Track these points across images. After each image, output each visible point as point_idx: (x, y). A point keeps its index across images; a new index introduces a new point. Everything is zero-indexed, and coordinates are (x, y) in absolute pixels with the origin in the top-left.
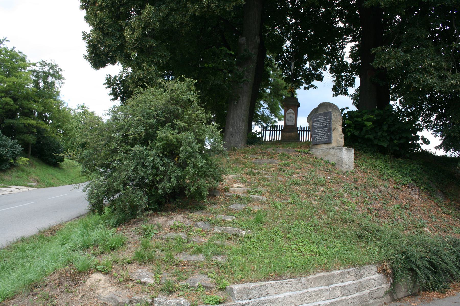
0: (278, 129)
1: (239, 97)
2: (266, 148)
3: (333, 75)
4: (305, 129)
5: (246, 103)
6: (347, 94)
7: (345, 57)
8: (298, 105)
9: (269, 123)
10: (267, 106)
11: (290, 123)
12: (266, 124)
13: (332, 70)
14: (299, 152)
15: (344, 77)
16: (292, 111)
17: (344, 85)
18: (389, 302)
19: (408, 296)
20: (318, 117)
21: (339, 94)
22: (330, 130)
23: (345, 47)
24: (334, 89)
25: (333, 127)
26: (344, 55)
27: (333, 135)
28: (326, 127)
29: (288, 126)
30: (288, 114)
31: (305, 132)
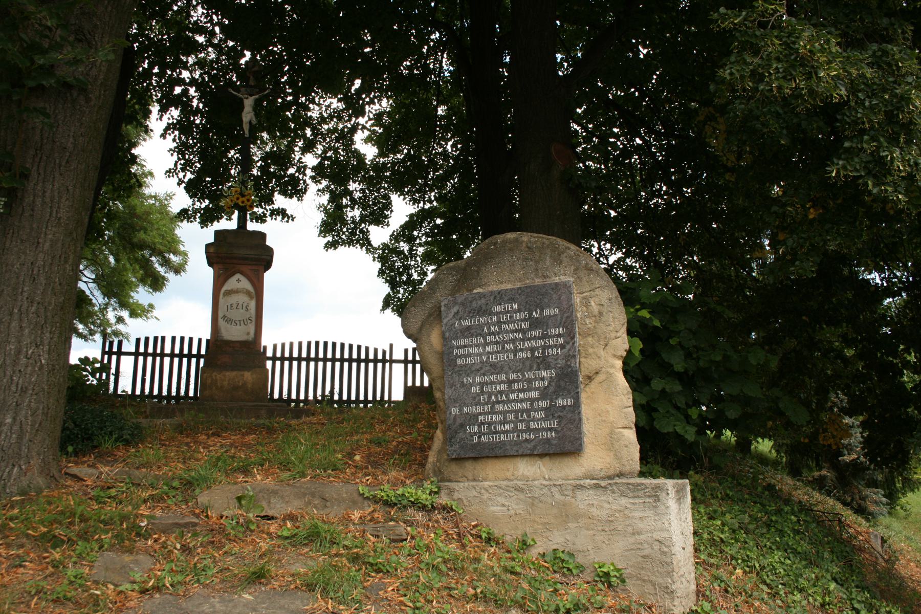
0: (168, 350)
1: (25, 176)
2: (189, 485)
3: (321, 187)
5: (63, 214)
6: (365, 242)
8: (268, 265)
9: (93, 323)
10: (93, 276)
11: (234, 333)
12: (86, 325)
14: (388, 504)
16: (245, 284)
20: (485, 311)
21: (344, 243)
22: (568, 381)
24: (326, 228)
25: (586, 365)
27: (586, 410)
28: (544, 363)
29: (229, 343)
30: (229, 293)
31: (295, 364)
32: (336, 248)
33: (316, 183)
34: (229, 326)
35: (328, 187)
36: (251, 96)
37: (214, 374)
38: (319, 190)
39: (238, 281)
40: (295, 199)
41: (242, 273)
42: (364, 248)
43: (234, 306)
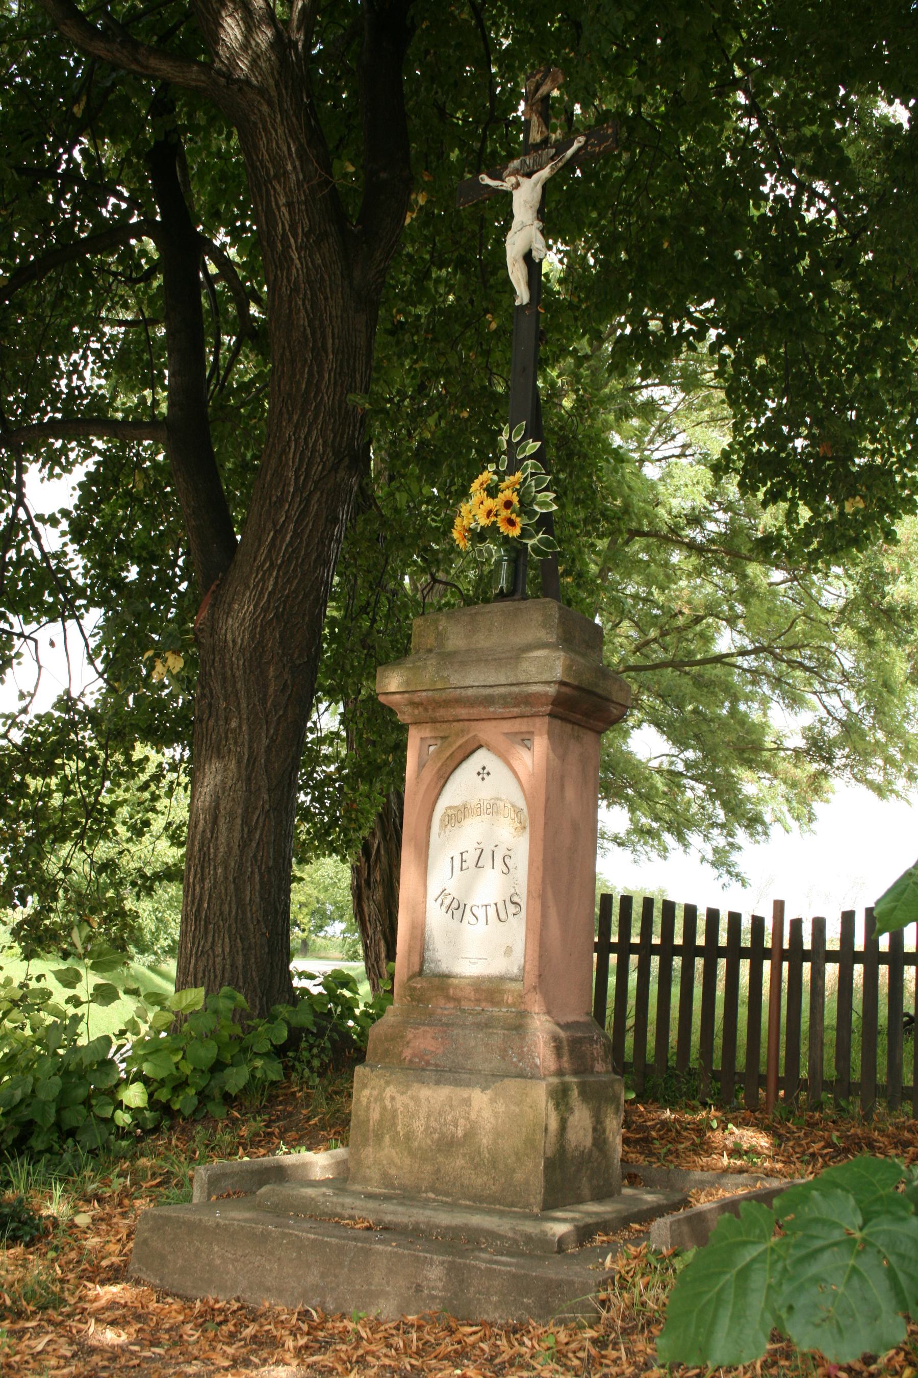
4: (833, 943)
36: (529, 175)
37: (390, 1091)
39: (483, 773)
43: (471, 858)
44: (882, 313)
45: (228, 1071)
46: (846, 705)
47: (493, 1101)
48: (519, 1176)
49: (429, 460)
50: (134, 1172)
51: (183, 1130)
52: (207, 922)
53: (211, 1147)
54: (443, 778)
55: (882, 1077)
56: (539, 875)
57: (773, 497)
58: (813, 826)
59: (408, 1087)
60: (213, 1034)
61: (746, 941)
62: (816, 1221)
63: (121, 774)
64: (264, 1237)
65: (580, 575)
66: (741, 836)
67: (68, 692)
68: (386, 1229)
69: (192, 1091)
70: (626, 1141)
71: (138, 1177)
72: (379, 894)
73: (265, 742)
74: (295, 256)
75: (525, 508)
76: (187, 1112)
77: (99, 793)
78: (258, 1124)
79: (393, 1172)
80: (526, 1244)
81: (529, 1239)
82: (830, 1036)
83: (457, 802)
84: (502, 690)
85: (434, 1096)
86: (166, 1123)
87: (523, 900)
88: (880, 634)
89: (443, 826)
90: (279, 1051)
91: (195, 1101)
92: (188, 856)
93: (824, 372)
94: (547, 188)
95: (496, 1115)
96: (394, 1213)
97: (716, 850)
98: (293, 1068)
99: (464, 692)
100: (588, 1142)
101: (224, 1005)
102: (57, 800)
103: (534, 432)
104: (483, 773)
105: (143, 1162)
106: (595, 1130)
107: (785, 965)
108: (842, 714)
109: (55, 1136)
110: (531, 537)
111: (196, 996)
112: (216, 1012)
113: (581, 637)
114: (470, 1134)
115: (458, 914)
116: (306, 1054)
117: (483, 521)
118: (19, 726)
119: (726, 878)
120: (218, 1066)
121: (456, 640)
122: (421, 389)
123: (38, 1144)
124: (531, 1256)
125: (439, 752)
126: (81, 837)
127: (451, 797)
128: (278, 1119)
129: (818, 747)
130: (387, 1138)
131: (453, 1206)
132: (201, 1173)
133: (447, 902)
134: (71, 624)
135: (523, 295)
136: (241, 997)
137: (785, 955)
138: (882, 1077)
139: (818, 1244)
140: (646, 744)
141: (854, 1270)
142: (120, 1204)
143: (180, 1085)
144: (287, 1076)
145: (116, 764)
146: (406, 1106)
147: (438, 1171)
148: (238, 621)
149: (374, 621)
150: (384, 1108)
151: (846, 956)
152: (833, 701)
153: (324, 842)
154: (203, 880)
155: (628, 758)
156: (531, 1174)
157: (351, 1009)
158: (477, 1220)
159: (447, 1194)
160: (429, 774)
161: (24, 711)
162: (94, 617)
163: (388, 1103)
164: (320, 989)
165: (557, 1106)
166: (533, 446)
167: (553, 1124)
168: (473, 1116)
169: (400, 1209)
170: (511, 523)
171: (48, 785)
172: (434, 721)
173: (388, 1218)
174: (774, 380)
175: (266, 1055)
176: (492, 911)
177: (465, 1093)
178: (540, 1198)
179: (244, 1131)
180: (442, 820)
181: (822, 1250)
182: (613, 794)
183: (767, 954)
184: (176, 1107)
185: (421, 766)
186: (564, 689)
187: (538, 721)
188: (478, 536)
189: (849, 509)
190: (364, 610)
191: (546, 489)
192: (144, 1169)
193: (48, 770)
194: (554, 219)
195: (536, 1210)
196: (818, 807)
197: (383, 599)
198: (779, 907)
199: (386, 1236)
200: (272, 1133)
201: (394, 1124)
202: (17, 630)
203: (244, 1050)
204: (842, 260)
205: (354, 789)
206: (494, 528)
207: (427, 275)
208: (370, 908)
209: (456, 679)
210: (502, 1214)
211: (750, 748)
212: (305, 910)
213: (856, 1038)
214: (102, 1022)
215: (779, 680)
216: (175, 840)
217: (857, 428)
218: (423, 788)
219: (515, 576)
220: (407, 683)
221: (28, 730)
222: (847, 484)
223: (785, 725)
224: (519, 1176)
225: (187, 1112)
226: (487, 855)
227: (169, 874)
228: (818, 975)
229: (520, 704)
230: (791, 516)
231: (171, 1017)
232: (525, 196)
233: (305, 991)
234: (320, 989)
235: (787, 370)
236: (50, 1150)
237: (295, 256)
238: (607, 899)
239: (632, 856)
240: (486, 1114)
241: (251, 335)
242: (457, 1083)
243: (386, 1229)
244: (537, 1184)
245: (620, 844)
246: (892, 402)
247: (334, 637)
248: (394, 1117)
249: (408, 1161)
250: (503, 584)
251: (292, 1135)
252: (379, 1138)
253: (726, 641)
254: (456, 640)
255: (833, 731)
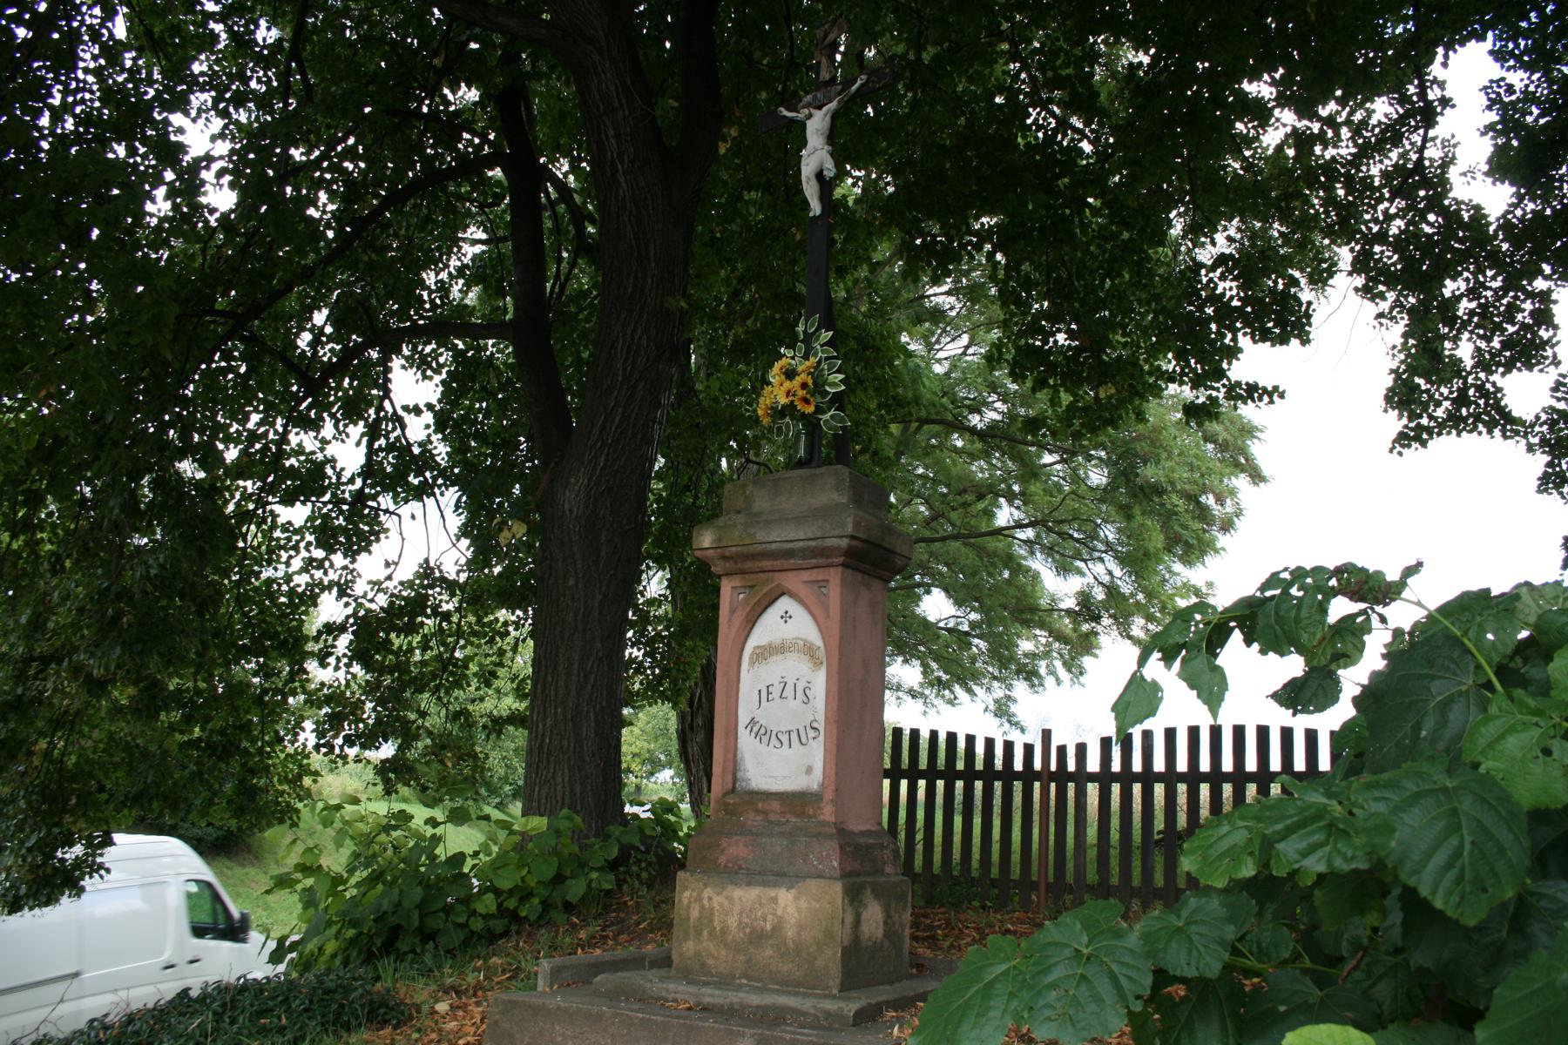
3: (1384, 306)
4: (1093, 765)
7: (1453, 174)
13: (1373, 277)
15: (1465, 305)
17: (1468, 363)
18: (417, 779)
19: (1016, 724)
21: (1442, 427)
23: (1445, 102)
24: (1402, 396)
26: (1447, 162)
32: (1424, 444)
33: (1372, 299)
34: (763, 748)
35: (1397, 304)
36: (820, 108)
37: (708, 892)
38: (1380, 315)
39: (786, 617)
40: (1295, 342)
41: (792, 595)
42: (1497, 432)
43: (776, 691)
44: (1126, 225)
45: (568, 883)
46: (1110, 573)
47: (796, 899)
48: (819, 963)
49: (741, 351)
50: (487, 969)
51: (529, 935)
52: (549, 754)
53: (553, 948)
54: (752, 621)
55: (1137, 880)
56: (835, 704)
57: (1040, 384)
58: (1082, 679)
59: (723, 888)
60: (555, 851)
61: (1018, 765)
62: (1050, 944)
63: (474, 634)
64: (600, 1016)
65: (875, 453)
66: (1020, 688)
67: (427, 561)
68: (704, 1009)
69: (536, 901)
70: (914, 938)
71: (490, 973)
72: (700, 737)
73: (599, 597)
74: (622, 179)
75: (818, 386)
76: (532, 918)
77: (454, 650)
78: (595, 928)
79: (711, 962)
80: (826, 1019)
81: (828, 1014)
82: (1092, 853)
83: (764, 642)
84: (801, 544)
85: (745, 896)
86: (514, 928)
87: (821, 726)
88: (1137, 511)
89: (752, 663)
90: (613, 866)
91: (540, 909)
92: (531, 707)
93: (1080, 276)
94: (835, 116)
95: (799, 910)
96: (712, 996)
97: (996, 701)
98: (625, 880)
99: (768, 546)
100: (880, 934)
101: (563, 825)
102: (417, 656)
103: (827, 323)
104: (786, 617)
105: (495, 960)
106: (885, 923)
107: (1053, 785)
108: (1106, 579)
109: (417, 941)
110: (824, 413)
111: (539, 823)
112: (557, 831)
113: (870, 496)
114: (777, 928)
115: (765, 739)
116: (635, 869)
117: (783, 400)
118: (385, 591)
119: (1007, 725)
120: (559, 879)
121: (761, 502)
122: (736, 294)
123: (403, 946)
124: (830, 1029)
125: (746, 600)
126: (438, 688)
127: (758, 638)
128: (612, 924)
129: (1087, 609)
130: (705, 933)
131: (763, 990)
132: (545, 965)
133: (756, 729)
134: (430, 502)
135: (816, 208)
136: (578, 819)
137: (1052, 777)
138: (1137, 880)
139: (1052, 961)
140: (936, 606)
141: (1083, 977)
142: (475, 995)
143: (526, 895)
144: (619, 887)
145: (470, 624)
146: (721, 905)
147: (750, 960)
148: (571, 498)
149: (696, 497)
150: (703, 907)
151: (1105, 778)
152: (1099, 569)
153: (653, 692)
154: (544, 719)
155: (925, 622)
156: (830, 961)
157: (675, 832)
158: (783, 1000)
159: (758, 980)
160: (739, 618)
161: (389, 578)
162: (451, 495)
163: (705, 902)
164: (649, 815)
165: (852, 902)
166: (826, 335)
167: (849, 920)
168: (780, 912)
169: (717, 992)
170: (806, 401)
171: (410, 643)
172: (743, 572)
173: (706, 1000)
174: (1037, 284)
175: (600, 869)
176: (794, 736)
177: (772, 892)
178: (838, 981)
179: (583, 935)
180: (751, 658)
181: (1055, 964)
182: (906, 651)
183: (1037, 776)
184: (523, 914)
185: (733, 611)
186: (855, 543)
187: (832, 570)
188: (779, 413)
189: (1102, 395)
190: (687, 488)
191: (838, 372)
192: (495, 967)
193: (411, 629)
194: (845, 146)
195: (835, 991)
196: (1087, 661)
197: (704, 477)
198: (1047, 735)
199: (704, 1014)
200: (606, 937)
201: (711, 921)
202: (383, 506)
203: (582, 865)
204: (1094, 178)
205: (680, 645)
206: (792, 406)
207: (740, 197)
208: (694, 749)
209: (760, 536)
210: (805, 995)
211: (1026, 609)
212: (637, 760)
213: (1114, 854)
214: (460, 840)
215: (1051, 549)
216: (520, 694)
217: (1110, 325)
218: (734, 629)
219: (811, 446)
220: (719, 539)
221: (392, 595)
222: (1103, 374)
223: (1060, 588)
224: (819, 963)
225: (532, 918)
226: (790, 688)
227: (515, 719)
228: (1081, 794)
229: (815, 556)
230: (1054, 401)
231: (518, 838)
232: (817, 124)
233: (635, 816)
234: (649, 815)
235: (1048, 276)
236: (413, 951)
237: (622, 179)
238: (897, 732)
239: (923, 708)
240: (791, 910)
241: (583, 248)
242: (766, 884)
243: (704, 1009)
244: (836, 969)
245: (914, 697)
246: (1140, 302)
247: (659, 513)
248: (712, 914)
249: (723, 952)
250: (802, 452)
251: (624, 937)
252: (698, 933)
253: (1005, 515)
254: (761, 502)
255: (1099, 594)
